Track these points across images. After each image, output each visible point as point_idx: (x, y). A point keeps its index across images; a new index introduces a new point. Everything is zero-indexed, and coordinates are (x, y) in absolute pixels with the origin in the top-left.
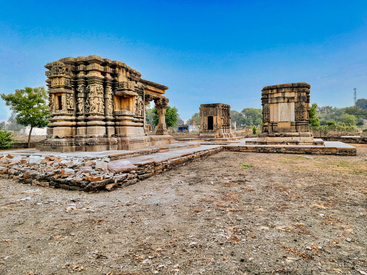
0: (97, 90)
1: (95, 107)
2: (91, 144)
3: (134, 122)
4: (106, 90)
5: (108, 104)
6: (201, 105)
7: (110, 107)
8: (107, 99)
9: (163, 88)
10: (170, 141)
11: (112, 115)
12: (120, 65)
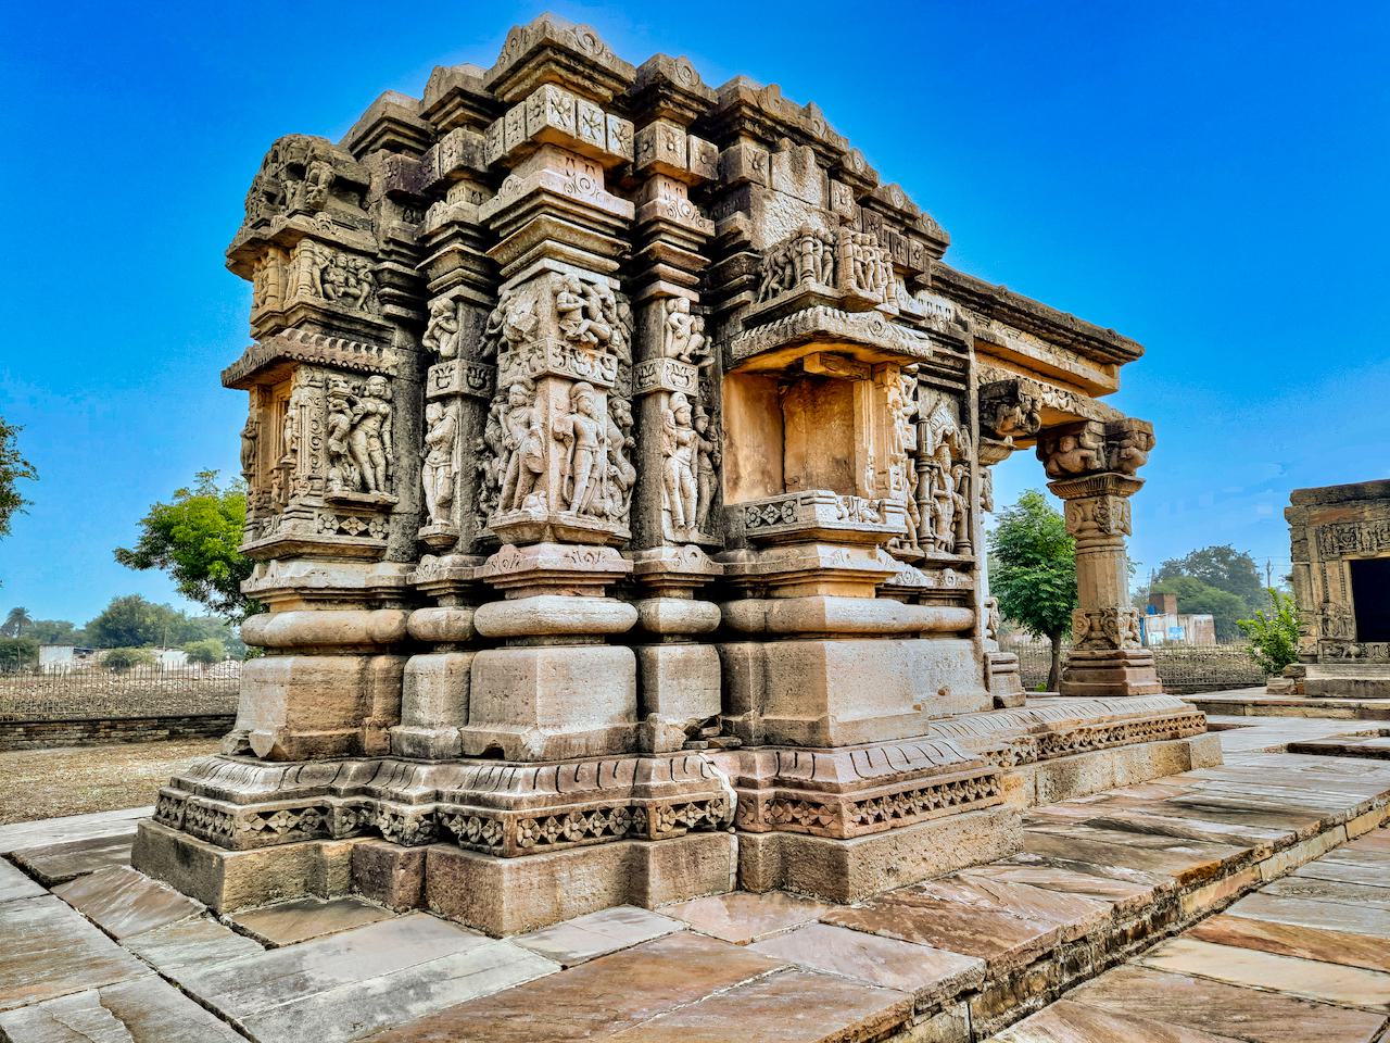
0: (562, 314)
1: (536, 468)
2: (472, 830)
3: (895, 596)
4: (653, 327)
5: (666, 445)
6: (1296, 498)
7: (677, 465)
8: (657, 402)
9: (1105, 351)
10: (1185, 748)
11: (695, 536)
12: (775, 111)
